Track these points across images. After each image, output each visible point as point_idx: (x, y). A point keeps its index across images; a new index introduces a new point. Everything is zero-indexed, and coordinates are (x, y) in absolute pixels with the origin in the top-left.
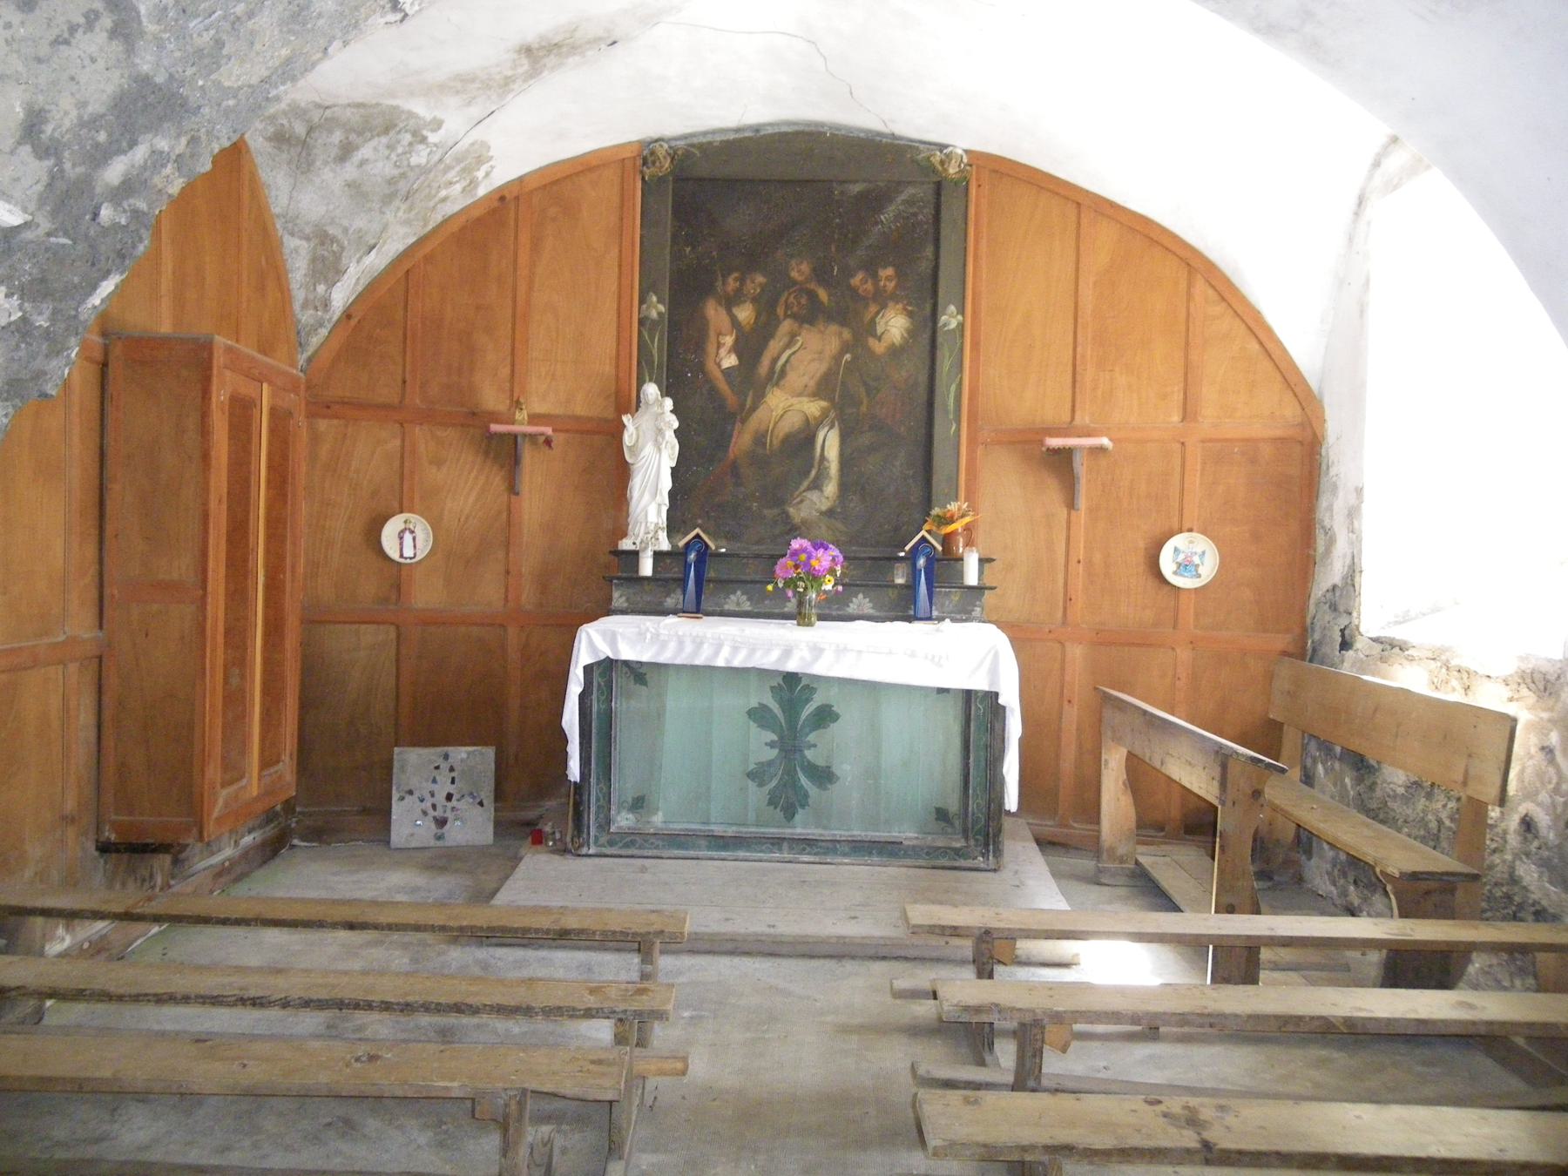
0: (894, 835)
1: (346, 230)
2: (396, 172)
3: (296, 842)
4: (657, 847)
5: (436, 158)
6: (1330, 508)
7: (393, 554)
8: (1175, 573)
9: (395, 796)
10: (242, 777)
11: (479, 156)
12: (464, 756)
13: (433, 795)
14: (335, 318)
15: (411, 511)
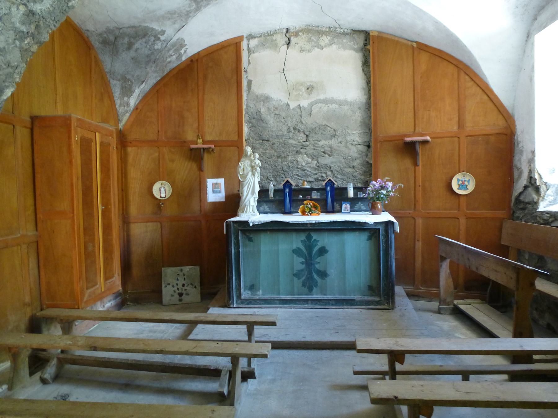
0: (352, 297)
1: (133, 76)
2: (150, 52)
3: (128, 303)
4: (260, 304)
5: (164, 45)
6: (520, 160)
7: (158, 197)
8: (458, 189)
9: (163, 286)
10: (96, 284)
11: (181, 44)
12: (188, 270)
13: (177, 285)
14: (132, 109)
15: (163, 180)
